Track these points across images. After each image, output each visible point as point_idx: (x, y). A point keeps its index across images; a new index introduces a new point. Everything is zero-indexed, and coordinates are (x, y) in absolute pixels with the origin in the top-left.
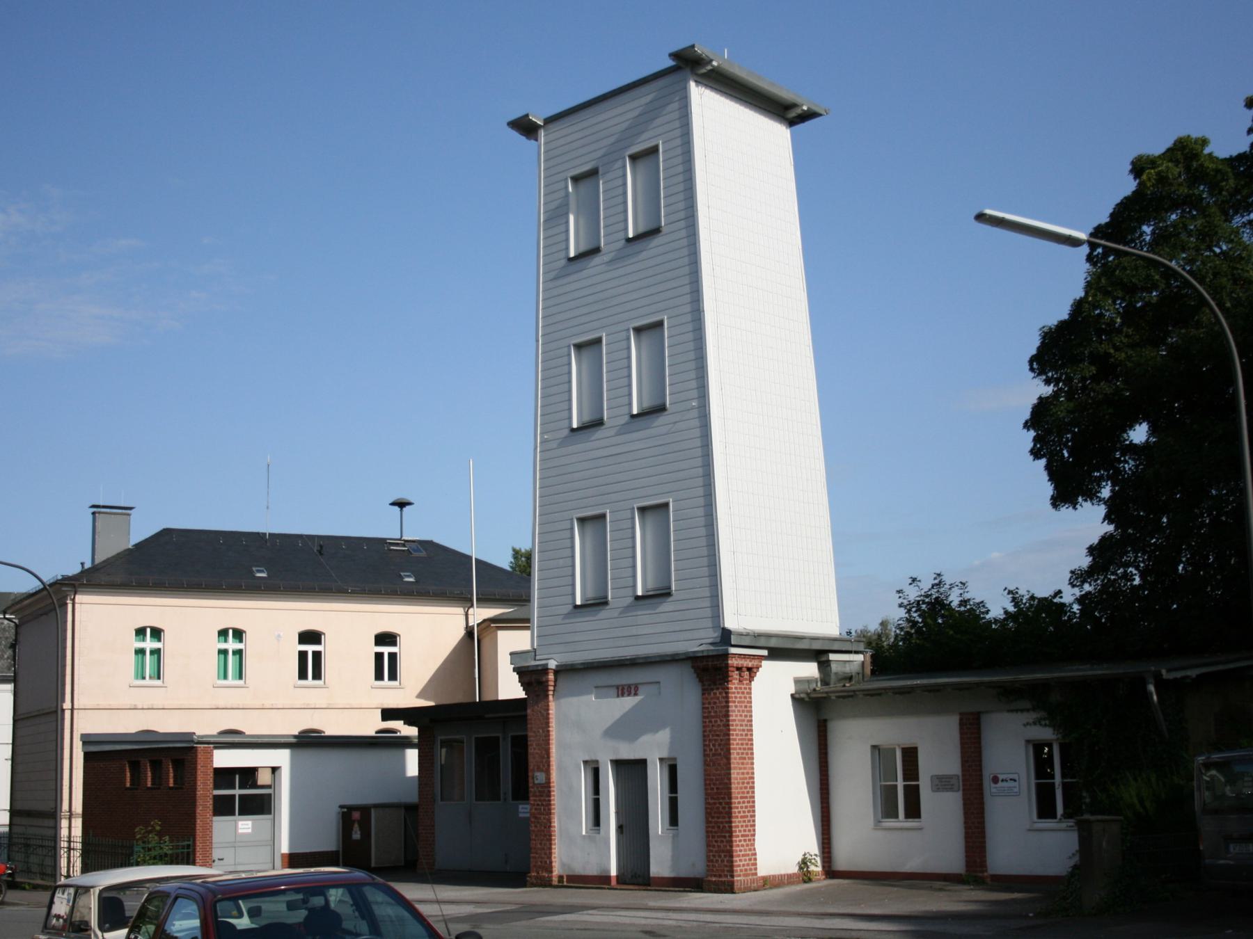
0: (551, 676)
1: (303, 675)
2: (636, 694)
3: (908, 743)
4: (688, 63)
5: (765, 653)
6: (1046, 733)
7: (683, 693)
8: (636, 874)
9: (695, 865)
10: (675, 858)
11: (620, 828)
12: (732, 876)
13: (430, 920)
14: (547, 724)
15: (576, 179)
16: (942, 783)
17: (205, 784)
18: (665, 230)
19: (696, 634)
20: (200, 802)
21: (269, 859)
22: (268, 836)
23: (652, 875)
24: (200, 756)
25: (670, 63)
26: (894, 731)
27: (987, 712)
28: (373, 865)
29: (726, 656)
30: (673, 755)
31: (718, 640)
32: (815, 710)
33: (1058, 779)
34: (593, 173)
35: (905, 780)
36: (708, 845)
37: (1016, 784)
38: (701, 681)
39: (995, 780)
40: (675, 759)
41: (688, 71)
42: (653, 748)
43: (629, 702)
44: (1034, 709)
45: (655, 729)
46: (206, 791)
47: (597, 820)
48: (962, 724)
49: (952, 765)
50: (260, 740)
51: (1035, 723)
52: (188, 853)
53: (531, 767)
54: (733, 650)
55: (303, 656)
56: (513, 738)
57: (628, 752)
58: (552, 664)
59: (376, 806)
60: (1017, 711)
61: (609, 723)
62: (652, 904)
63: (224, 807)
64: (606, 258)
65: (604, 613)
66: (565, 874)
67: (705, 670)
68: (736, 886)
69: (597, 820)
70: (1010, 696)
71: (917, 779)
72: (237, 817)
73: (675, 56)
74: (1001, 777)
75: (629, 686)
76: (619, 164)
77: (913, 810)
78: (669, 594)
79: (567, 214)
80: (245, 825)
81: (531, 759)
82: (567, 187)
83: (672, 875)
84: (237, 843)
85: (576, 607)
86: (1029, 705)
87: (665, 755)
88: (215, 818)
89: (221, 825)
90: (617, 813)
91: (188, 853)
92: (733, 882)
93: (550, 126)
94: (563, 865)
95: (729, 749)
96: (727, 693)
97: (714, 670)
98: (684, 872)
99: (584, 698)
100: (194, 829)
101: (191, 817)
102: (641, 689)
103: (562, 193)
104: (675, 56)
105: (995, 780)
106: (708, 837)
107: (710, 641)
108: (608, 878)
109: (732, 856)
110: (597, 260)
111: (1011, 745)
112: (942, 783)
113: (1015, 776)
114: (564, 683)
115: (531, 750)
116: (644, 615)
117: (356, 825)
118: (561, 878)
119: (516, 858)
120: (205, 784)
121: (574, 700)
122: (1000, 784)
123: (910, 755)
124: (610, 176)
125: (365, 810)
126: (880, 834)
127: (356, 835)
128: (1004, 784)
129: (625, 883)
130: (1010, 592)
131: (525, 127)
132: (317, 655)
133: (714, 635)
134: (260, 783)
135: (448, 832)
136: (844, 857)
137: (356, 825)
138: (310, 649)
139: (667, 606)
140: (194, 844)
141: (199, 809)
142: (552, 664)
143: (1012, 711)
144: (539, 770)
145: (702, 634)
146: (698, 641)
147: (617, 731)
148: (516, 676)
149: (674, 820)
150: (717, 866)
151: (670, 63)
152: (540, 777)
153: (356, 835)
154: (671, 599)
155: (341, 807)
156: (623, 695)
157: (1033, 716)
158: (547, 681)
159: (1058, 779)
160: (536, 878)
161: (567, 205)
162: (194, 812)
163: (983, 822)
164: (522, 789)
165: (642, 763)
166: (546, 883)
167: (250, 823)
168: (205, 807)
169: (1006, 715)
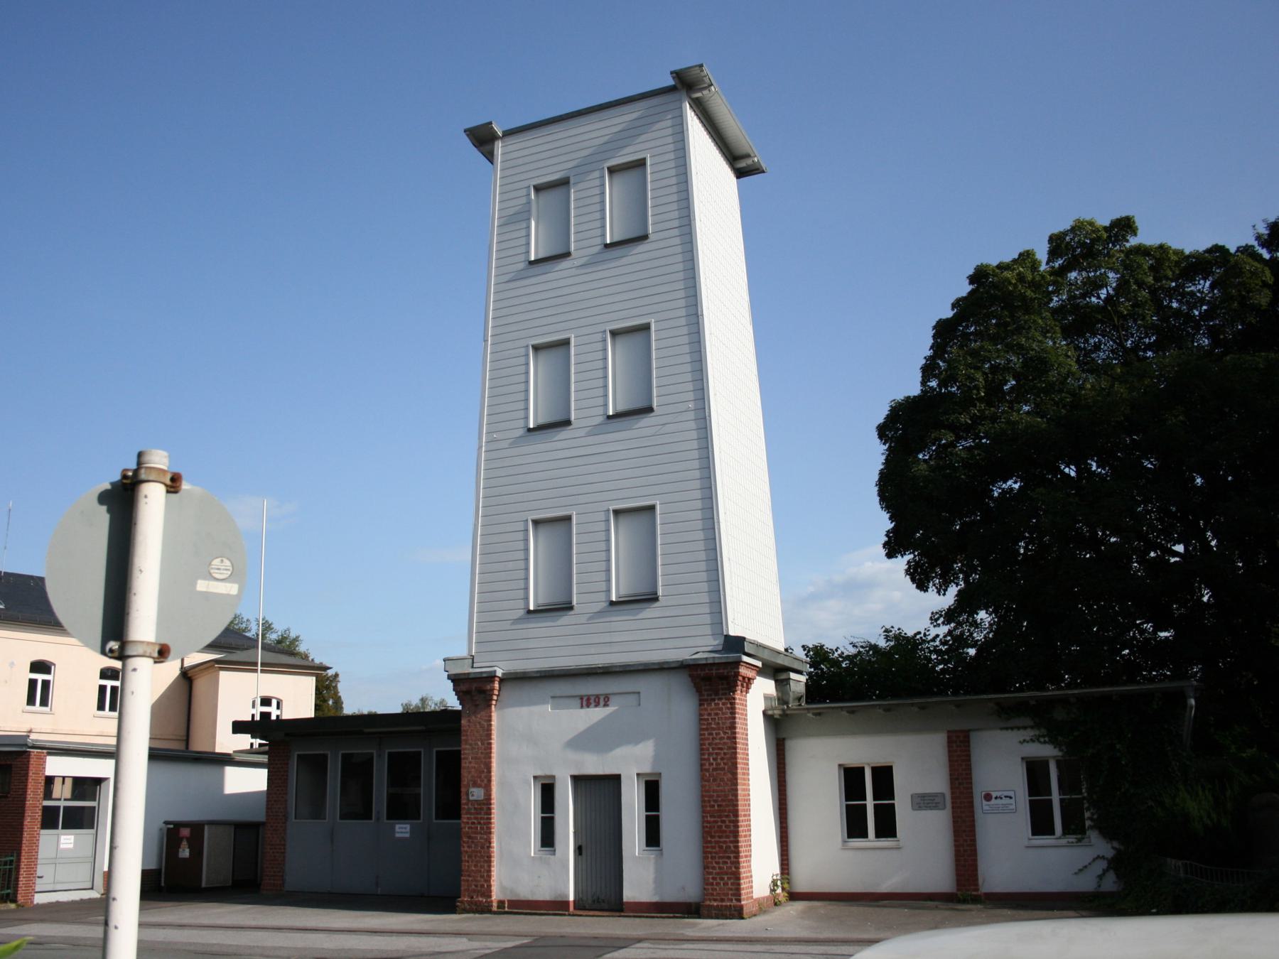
0: (497, 685)
1: (31, 700)
2: (606, 705)
3: (881, 761)
4: (686, 83)
5: (759, 664)
6: (1046, 751)
7: (678, 708)
8: (602, 895)
9: (686, 886)
10: (658, 881)
11: (579, 850)
12: (739, 900)
13: (857, 948)
14: (489, 736)
15: (538, 189)
16: (924, 802)
17: (35, 793)
18: (652, 237)
19: (690, 642)
20: (28, 813)
21: (88, 877)
22: (90, 853)
23: (625, 899)
24: (32, 761)
25: (670, 82)
26: (865, 750)
27: (978, 730)
28: (204, 885)
29: (738, 663)
30: (657, 770)
31: (720, 648)
32: (780, 726)
33: (1056, 797)
34: (564, 183)
35: (875, 798)
36: (706, 867)
37: (1012, 801)
38: (699, 690)
39: (988, 797)
40: (553, 777)
41: (684, 94)
42: (630, 763)
43: (596, 714)
44: (1032, 727)
45: (636, 739)
46: (35, 802)
47: (548, 838)
48: (950, 742)
49: (938, 783)
50: (94, 748)
51: (1032, 741)
52: (10, 870)
53: (465, 781)
54: (745, 659)
55: (33, 683)
56: (390, 754)
57: (594, 765)
58: (499, 673)
59: (211, 823)
60: (1012, 729)
61: (571, 736)
62: (690, 933)
63: (50, 819)
64: (577, 263)
65: (566, 619)
66: (506, 897)
67: (707, 679)
68: (746, 910)
69: (548, 838)
70: (1007, 714)
71: (892, 797)
72: (60, 831)
73: (677, 75)
74: (994, 795)
75: (598, 697)
76: (597, 174)
77: (887, 827)
78: (656, 599)
79: (529, 219)
80: (67, 840)
81: (464, 773)
82: (529, 195)
83: (655, 899)
84: (59, 859)
85: (529, 612)
86: (1029, 722)
87: (647, 769)
88: (43, 832)
89: (46, 836)
90: (575, 833)
91: (10, 870)
92: (741, 907)
93: (506, 139)
94: (503, 888)
95: (736, 763)
96: (733, 704)
97: (715, 677)
98: (671, 896)
99: (536, 709)
100: (20, 843)
101: (18, 829)
102: (613, 700)
103: (524, 200)
104: (677, 75)
105: (988, 797)
106: (705, 858)
107: (710, 648)
108: (567, 903)
109: (739, 879)
110: (565, 264)
111: (1003, 762)
112: (924, 802)
113: (1011, 794)
114: (510, 692)
115: (464, 764)
116: (623, 622)
117: (185, 843)
118: (501, 903)
119: (442, 878)
120: (35, 793)
121: (524, 710)
122: (993, 801)
123: (884, 776)
124: (581, 186)
125: (197, 828)
126: (850, 854)
127: (185, 853)
128: (999, 801)
129: (584, 909)
130: (886, 631)
131: (483, 139)
132: (46, 684)
133: (717, 642)
134: (54, 796)
135: (304, 846)
136: (804, 880)
137: (185, 843)
138: (40, 677)
139: (650, 612)
140: (19, 860)
141: (27, 821)
142: (499, 673)
143: (1007, 729)
144: (475, 785)
145: (699, 641)
146: (701, 647)
147: (582, 742)
148: (451, 685)
149: (653, 837)
150: (718, 892)
151: (670, 82)
152: (477, 794)
153: (185, 853)
154: (657, 604)
155: (166, 823)
156: (588, 706)
157: (1029, 734)
158: (493, 689)
159: (1056, 797)
160: (470, 903)
161: (529, 211)
162: (22, 824)
163: (974, 840)
164: (451, 804)
165: (615, 779)
166: (485, 909)
167: (72, 837)
168: (33, 818)
169: (998, 733)
